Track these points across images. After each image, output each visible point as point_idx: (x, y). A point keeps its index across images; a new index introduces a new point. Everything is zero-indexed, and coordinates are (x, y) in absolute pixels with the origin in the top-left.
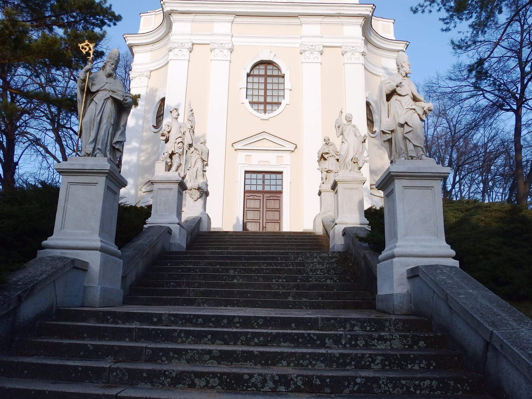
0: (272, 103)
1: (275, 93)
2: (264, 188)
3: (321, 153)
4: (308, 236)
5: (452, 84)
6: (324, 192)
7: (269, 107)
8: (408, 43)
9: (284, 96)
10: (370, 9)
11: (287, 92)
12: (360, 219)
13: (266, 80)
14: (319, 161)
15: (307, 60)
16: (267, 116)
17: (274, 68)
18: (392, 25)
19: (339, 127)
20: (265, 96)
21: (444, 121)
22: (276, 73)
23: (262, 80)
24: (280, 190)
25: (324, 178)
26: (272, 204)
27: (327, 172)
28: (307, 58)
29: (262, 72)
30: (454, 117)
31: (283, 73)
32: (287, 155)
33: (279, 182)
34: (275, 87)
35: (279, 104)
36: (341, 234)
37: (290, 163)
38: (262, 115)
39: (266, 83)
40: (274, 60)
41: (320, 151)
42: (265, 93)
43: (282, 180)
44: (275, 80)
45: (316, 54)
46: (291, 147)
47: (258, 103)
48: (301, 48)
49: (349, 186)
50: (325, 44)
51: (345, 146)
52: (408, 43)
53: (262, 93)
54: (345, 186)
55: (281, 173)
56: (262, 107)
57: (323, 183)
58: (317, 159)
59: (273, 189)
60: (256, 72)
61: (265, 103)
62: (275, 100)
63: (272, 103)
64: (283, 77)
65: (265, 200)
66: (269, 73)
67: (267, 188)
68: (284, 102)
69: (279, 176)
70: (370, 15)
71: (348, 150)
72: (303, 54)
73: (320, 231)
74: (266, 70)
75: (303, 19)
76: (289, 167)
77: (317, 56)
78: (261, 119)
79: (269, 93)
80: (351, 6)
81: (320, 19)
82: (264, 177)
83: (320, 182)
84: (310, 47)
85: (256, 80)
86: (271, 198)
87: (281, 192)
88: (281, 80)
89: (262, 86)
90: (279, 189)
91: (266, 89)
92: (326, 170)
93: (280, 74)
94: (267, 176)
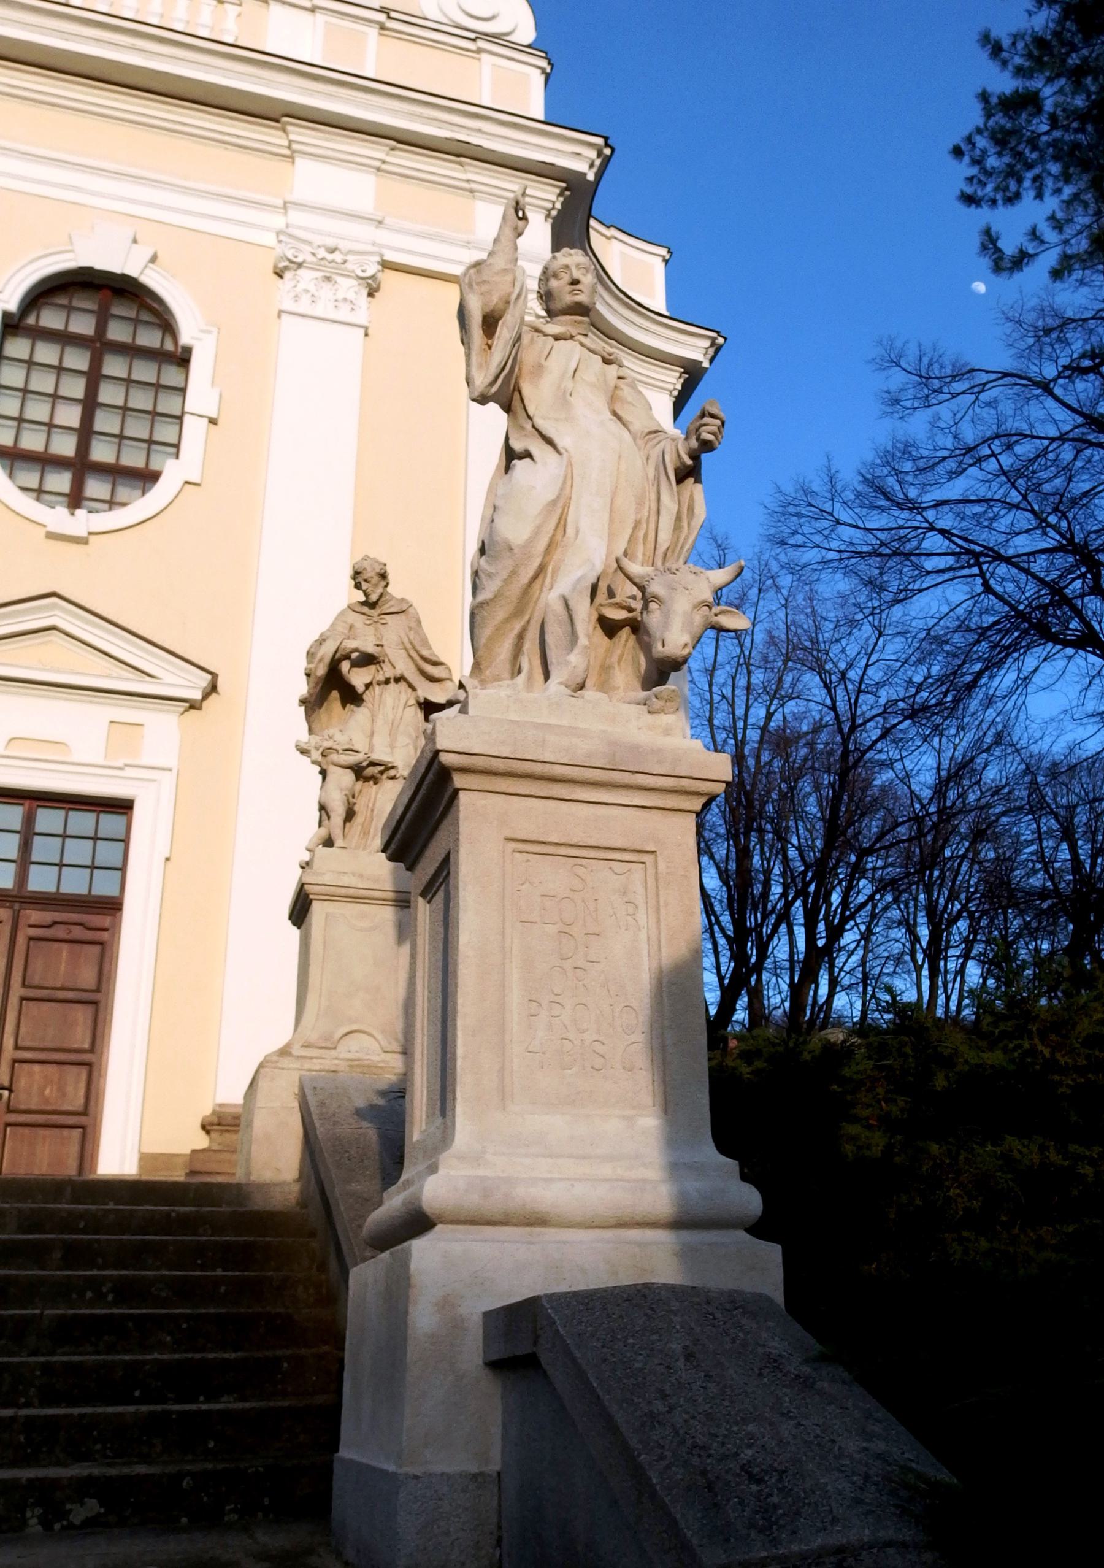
0: (115, 472)
1: (137, 428)
2: (22, 876)
3: (328, 651)
4: (187, 1224)
5: (877, 520)
6: (332, 898)
7: (95, 487)
8: (721, 340)
9: (177, 446)
10: (592, 154)
11: (193, 430)
12: (676, 1169)
13: (96, 364)
14: (313, 704)
15: (304, 307)
16: (81, 522)
17: (145, 316)
18: (660, 267)
19: (490, 323)
20: (85, 433)
21: (811, 680)
22: (149, 338)
23: (78, 359)
24: (111, 891)
25: (338, 811)
26: (61, 966)
27: (358, 771)
28: (306, 299)
29: (83, 325)
30: (850, 665)
31: (185, 339)
32: (162, 729)
33: (107, 853)
34: (141, 400)
35: (148, 478)
36: (472, 1352)
37: (173, 763)
38: (59, 518)
39: (94, 377)
40: (152, 279)
41: (321, 641)
42: (87, 418)
43: (126, 841)
44: (144, 371)
45: (349, 288)
46: (192, 686)
47: (45, 461)
48: (279, 250)
49: (573, 820)
50: (390, 256)
51: (538, 477)
52: (721, 340)
53: (70, 416)
54: (532, 815)
55: (123, 807)
56: (61, 481)
57: (329, 842)
58: (302, 688)
59: (74, 884)
60: (50, 319)
61: (81, 466)
62: (133, 458)
63: (115, 472)
64: (183, 359)
65: (21, 941)
66: (117, 332)
67: (41, 881)
68: (173, 473)
69: (110, 823)
70: (591, 177)
71: (559, 511)
72: (288, 275)
73: (274, 1161)
74: (103, 320)
75: (301, 134)
76: (167, 781)
77: (351, 295)
78: (52, 536)
79: (105, 422)
80: (515, 126)
81: (376, 151)
82: (29, 820)
83: (309, 828)
84: (322, 253)
85: (47, 353)
86: (60, 932)
87: (113, 906)
88: (171, 375)
89: (76, 388)
90: (104, 886)
91: (90, 405)
92: (352, 759)
93: (169, 346)
94: (48, 819)
